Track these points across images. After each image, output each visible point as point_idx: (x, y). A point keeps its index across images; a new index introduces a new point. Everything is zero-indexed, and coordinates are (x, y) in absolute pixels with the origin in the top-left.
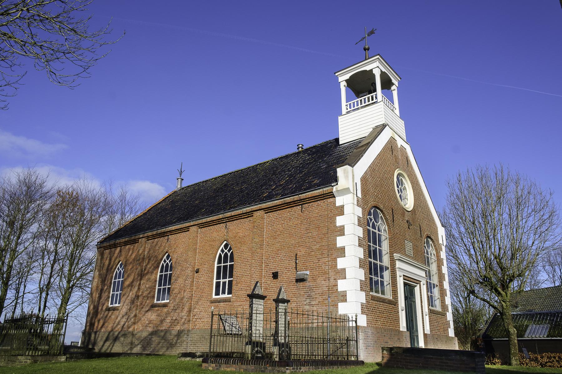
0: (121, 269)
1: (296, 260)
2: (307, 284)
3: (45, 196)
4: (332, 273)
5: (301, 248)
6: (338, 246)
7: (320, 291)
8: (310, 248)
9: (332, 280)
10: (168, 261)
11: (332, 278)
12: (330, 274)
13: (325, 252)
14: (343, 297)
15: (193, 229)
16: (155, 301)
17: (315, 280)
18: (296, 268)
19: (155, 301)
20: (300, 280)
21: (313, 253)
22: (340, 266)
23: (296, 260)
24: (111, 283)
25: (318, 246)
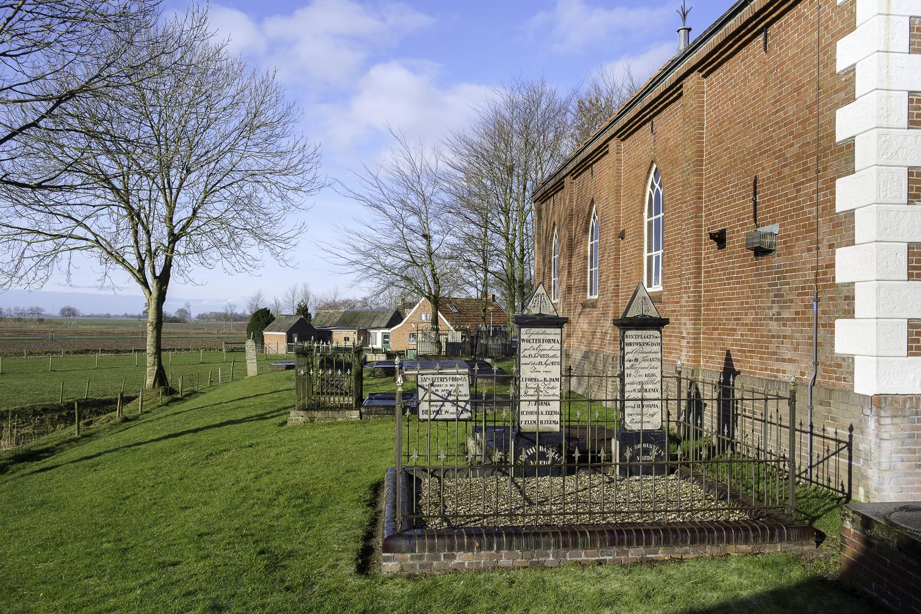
0: (657, 186)
1: (755, 194)
2: (776, 260)
3: (563, 110)
4: (824, 229)
5: (763, 160)
6: (838, 281)
7: (797, 282)
8: (781, 156)
9: (824, 250)
10: (657, 186)
11: (825, 243)
12: (821, 230)
13: (811, 162)
14: (843, 228)
15: (613, 144)
16: (589, 297)
17: (789, 249)
18: (755, 216)
19: (589, 297)
20: (761, 252)
21: (786, 170)
22: (840, 348)
23: (755, 194)
24: (550, 262)
25: (795, 149)
